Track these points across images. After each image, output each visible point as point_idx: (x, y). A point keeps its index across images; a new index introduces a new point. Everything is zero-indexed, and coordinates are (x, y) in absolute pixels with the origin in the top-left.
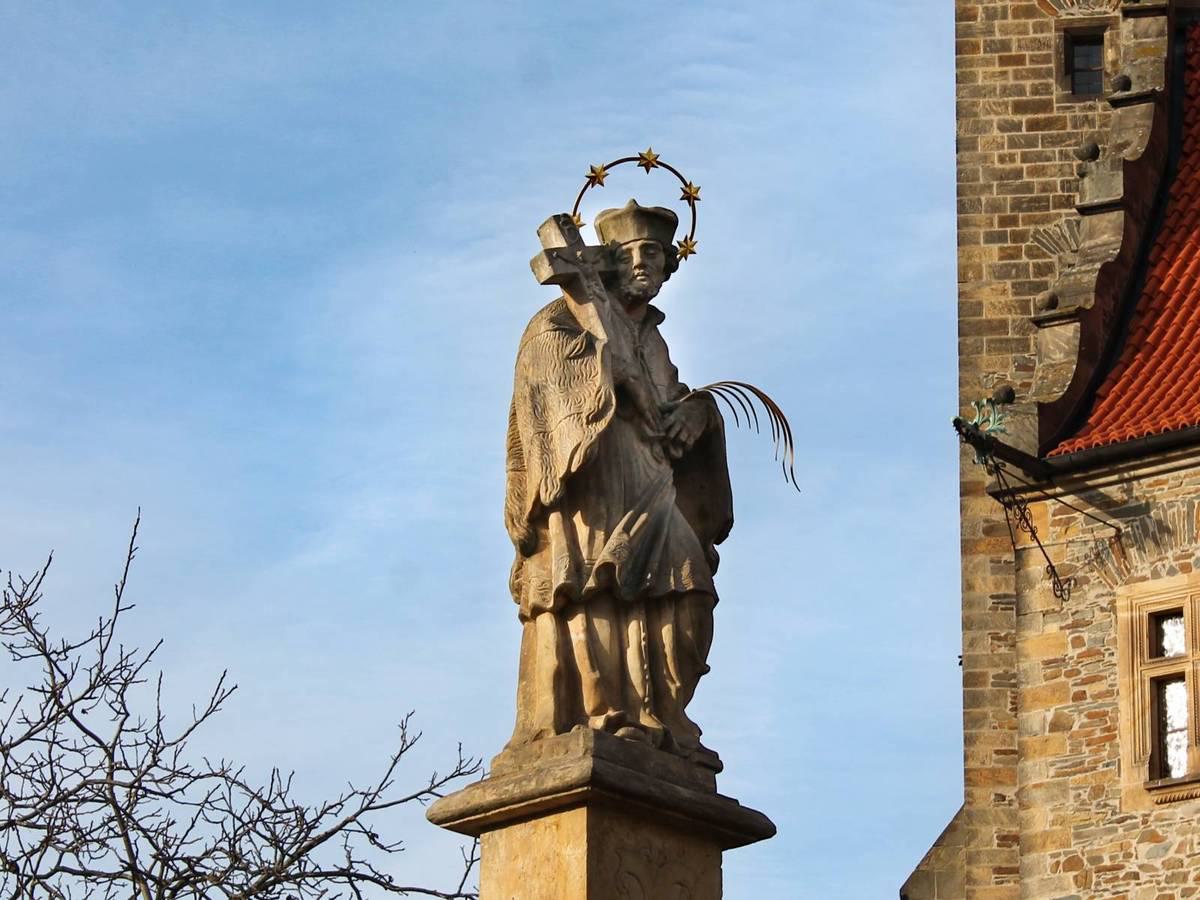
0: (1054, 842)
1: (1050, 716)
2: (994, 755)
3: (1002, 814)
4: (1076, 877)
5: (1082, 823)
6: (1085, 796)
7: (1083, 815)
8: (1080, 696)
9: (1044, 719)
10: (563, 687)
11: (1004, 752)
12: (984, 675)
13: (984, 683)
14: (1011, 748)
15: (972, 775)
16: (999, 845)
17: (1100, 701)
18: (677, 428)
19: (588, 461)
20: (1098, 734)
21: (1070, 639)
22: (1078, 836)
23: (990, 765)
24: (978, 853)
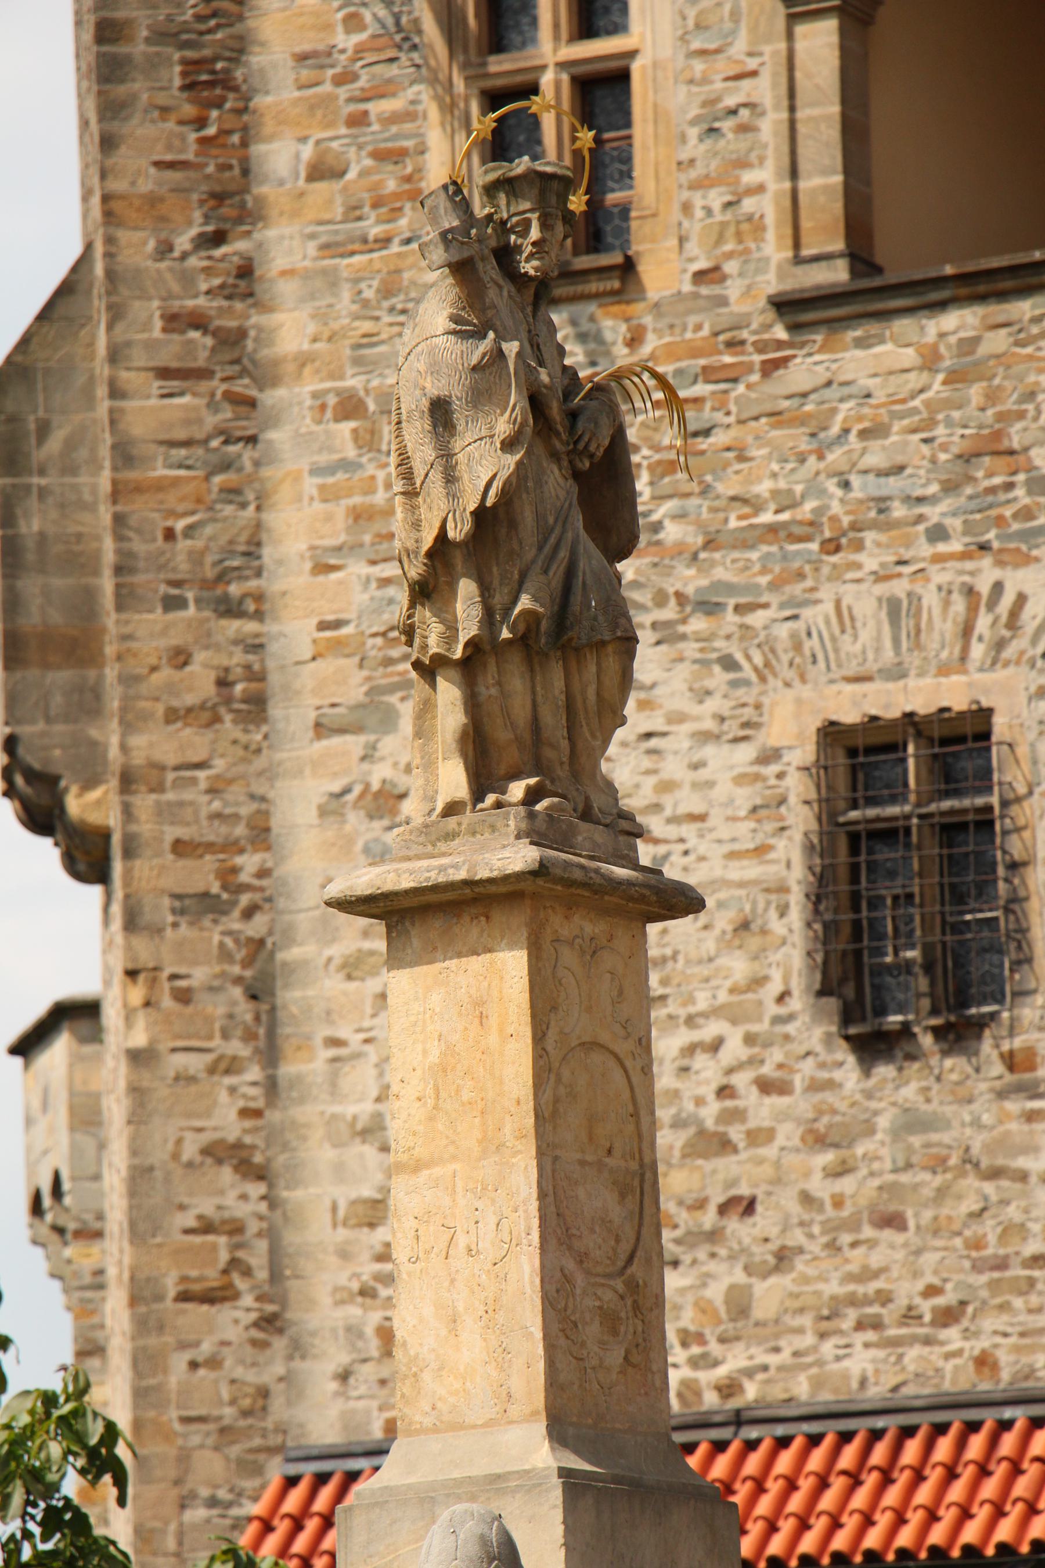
0: (317, 371)
1: (307, 152)
2: (152, 170)
3: (168, 276)
4: (355, 431)
5: (365, 340)
6: (369, 294)
7: (367, 326)
8: (359, 120)
9: (297, 156)
10: (471, 747)
11: (171, 165)
12: (128, 23)
13: (130, 39)
14: (182, 157)
15: (116, 206)
16: (164, 330)
17: (394, 129)
18: (586, 438)
19: (507, 495)
20: (391, 185)
21: (340, 15)
22: (357, 361)
23: (145, 186)
24: (128, 344)
